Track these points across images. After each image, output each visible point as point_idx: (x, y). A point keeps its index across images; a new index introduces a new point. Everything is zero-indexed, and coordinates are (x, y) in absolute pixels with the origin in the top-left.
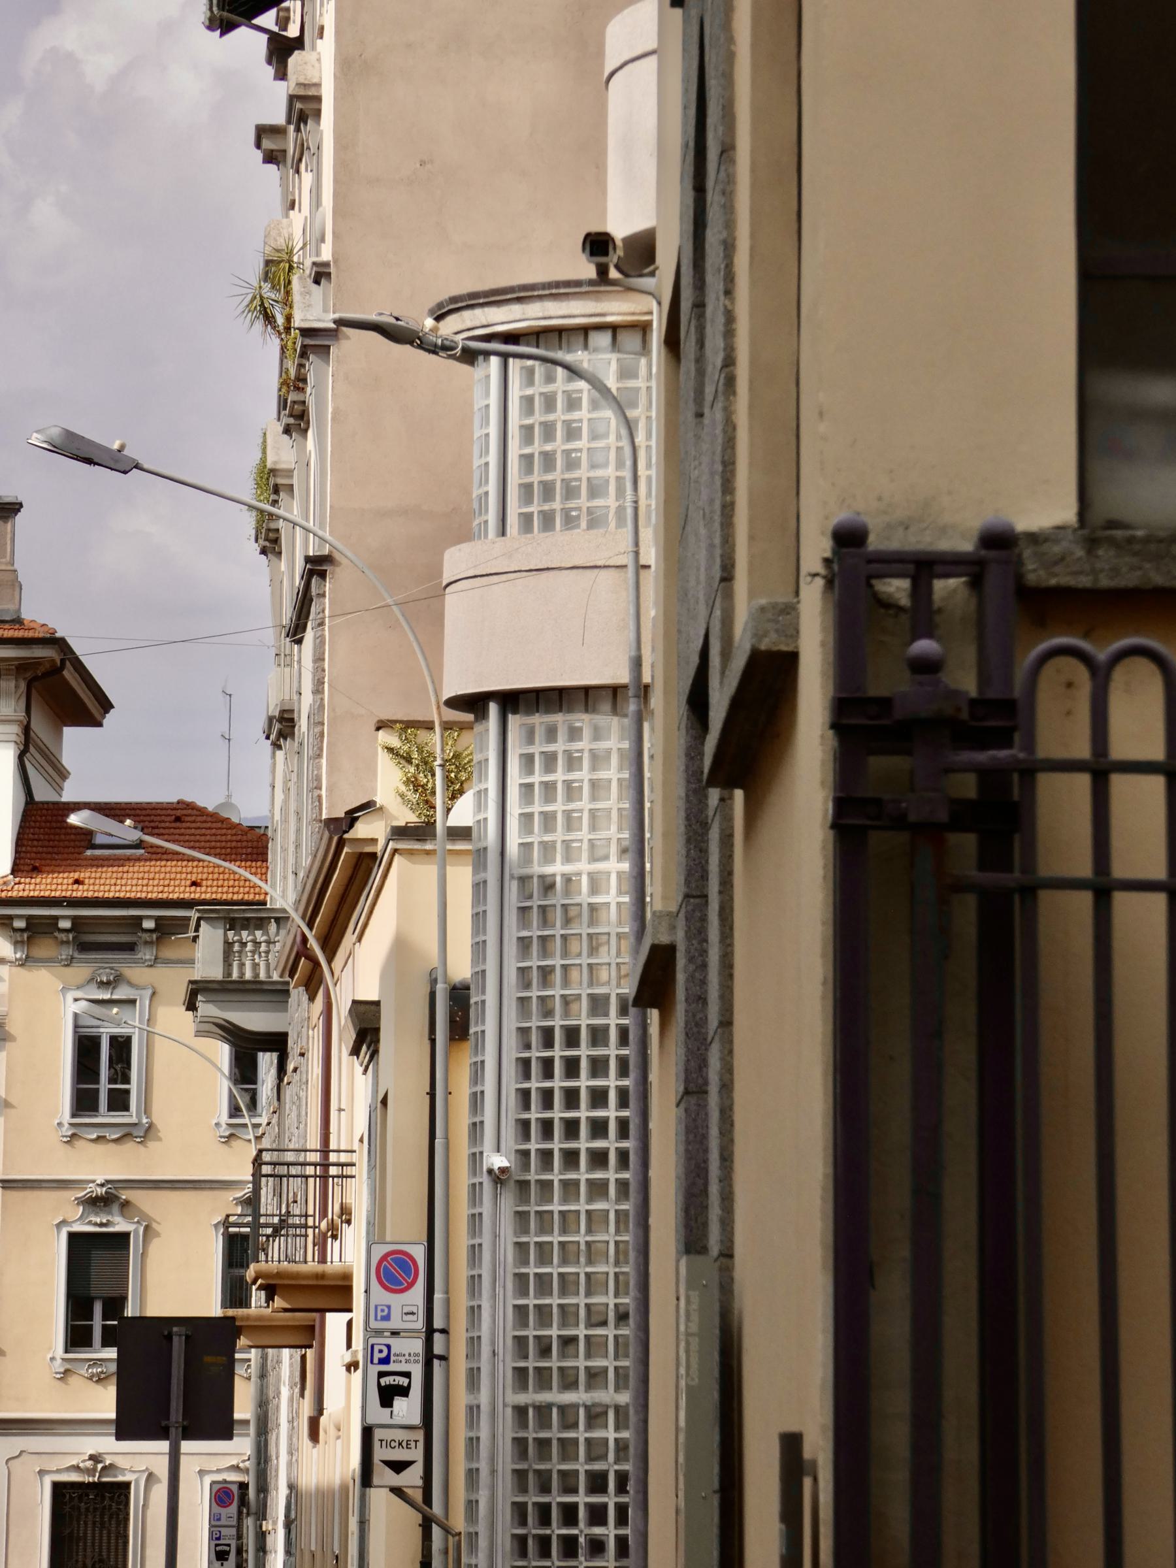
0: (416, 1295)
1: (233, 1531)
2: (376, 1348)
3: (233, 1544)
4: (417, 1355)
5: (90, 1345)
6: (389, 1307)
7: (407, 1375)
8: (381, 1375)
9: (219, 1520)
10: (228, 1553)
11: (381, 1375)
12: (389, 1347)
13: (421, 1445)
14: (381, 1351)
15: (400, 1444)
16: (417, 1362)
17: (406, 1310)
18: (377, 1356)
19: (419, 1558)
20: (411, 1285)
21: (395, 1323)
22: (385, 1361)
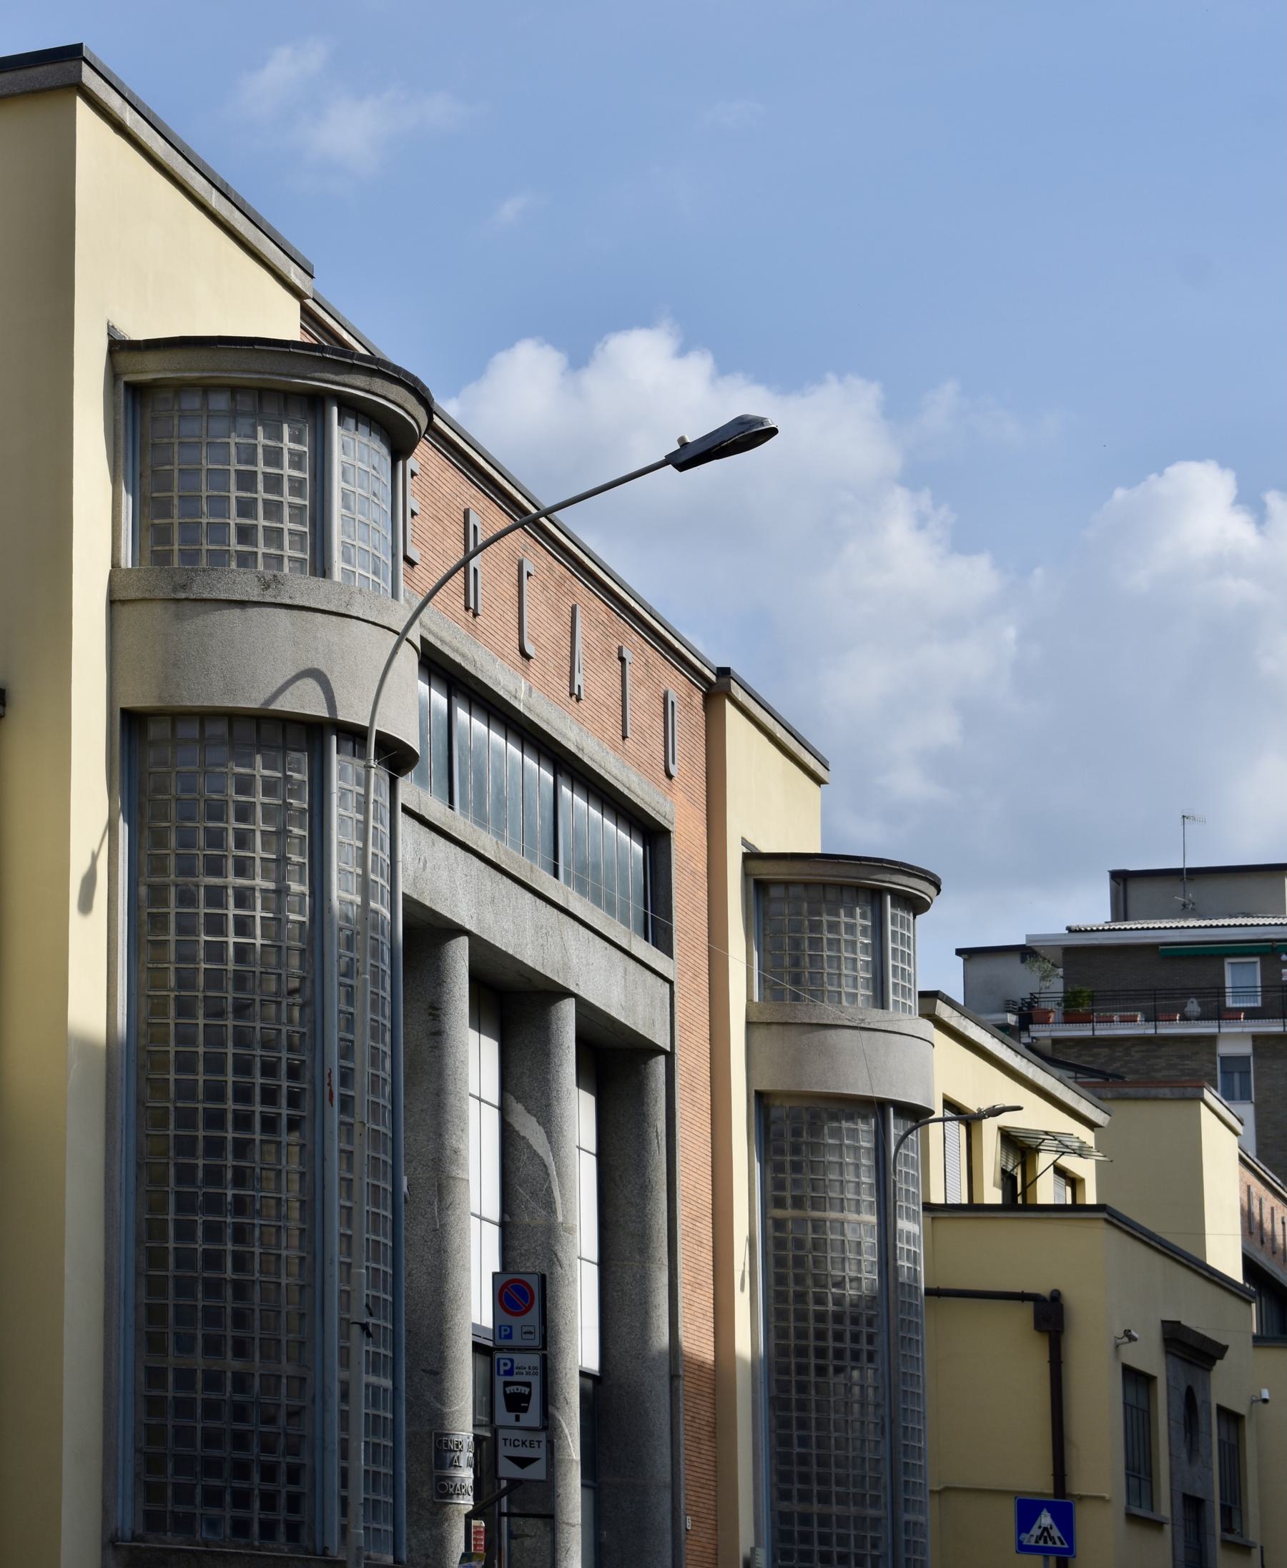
0: (534, 1315)
1: (533, 1360)
2: (502, 1362)
3: (536, 1381)
4: (535, 1368)
5: (249, 921)
6: (511, 1327)
7: (528, 1385)
8: (507, 1384)
9: (509, 1336)
10: (527, 1398)
11: (507, 1384)
12: (512, 1361)
13: (543, 1445)
14: (505, 1364)
15: (523, 1443)
16: (535, 1374)
17: (525, 1329)
18: (502, 1368)
19: (1019, 1302)
20: (528, 1309)
21: (516, 1341)
22: (509, 1373)
